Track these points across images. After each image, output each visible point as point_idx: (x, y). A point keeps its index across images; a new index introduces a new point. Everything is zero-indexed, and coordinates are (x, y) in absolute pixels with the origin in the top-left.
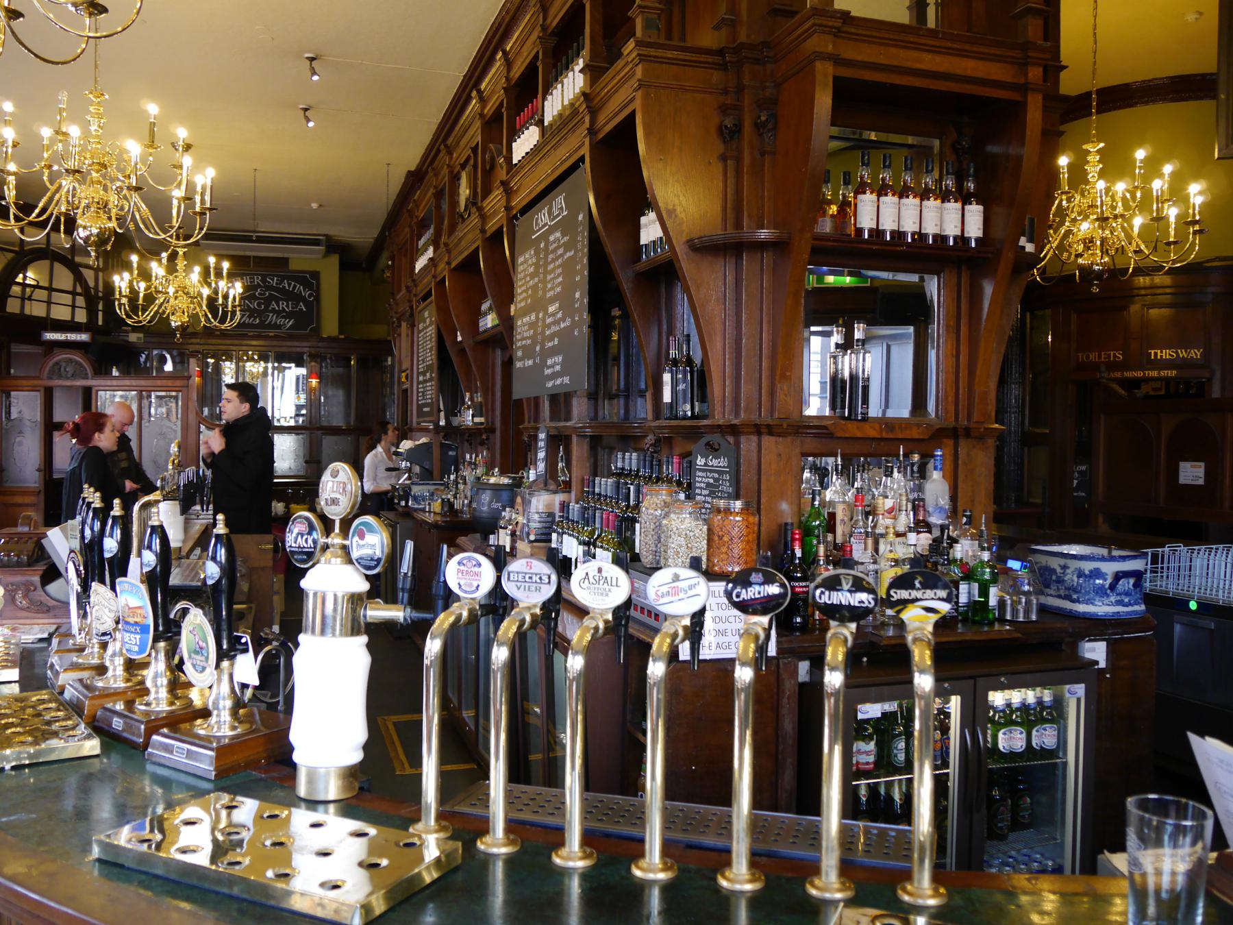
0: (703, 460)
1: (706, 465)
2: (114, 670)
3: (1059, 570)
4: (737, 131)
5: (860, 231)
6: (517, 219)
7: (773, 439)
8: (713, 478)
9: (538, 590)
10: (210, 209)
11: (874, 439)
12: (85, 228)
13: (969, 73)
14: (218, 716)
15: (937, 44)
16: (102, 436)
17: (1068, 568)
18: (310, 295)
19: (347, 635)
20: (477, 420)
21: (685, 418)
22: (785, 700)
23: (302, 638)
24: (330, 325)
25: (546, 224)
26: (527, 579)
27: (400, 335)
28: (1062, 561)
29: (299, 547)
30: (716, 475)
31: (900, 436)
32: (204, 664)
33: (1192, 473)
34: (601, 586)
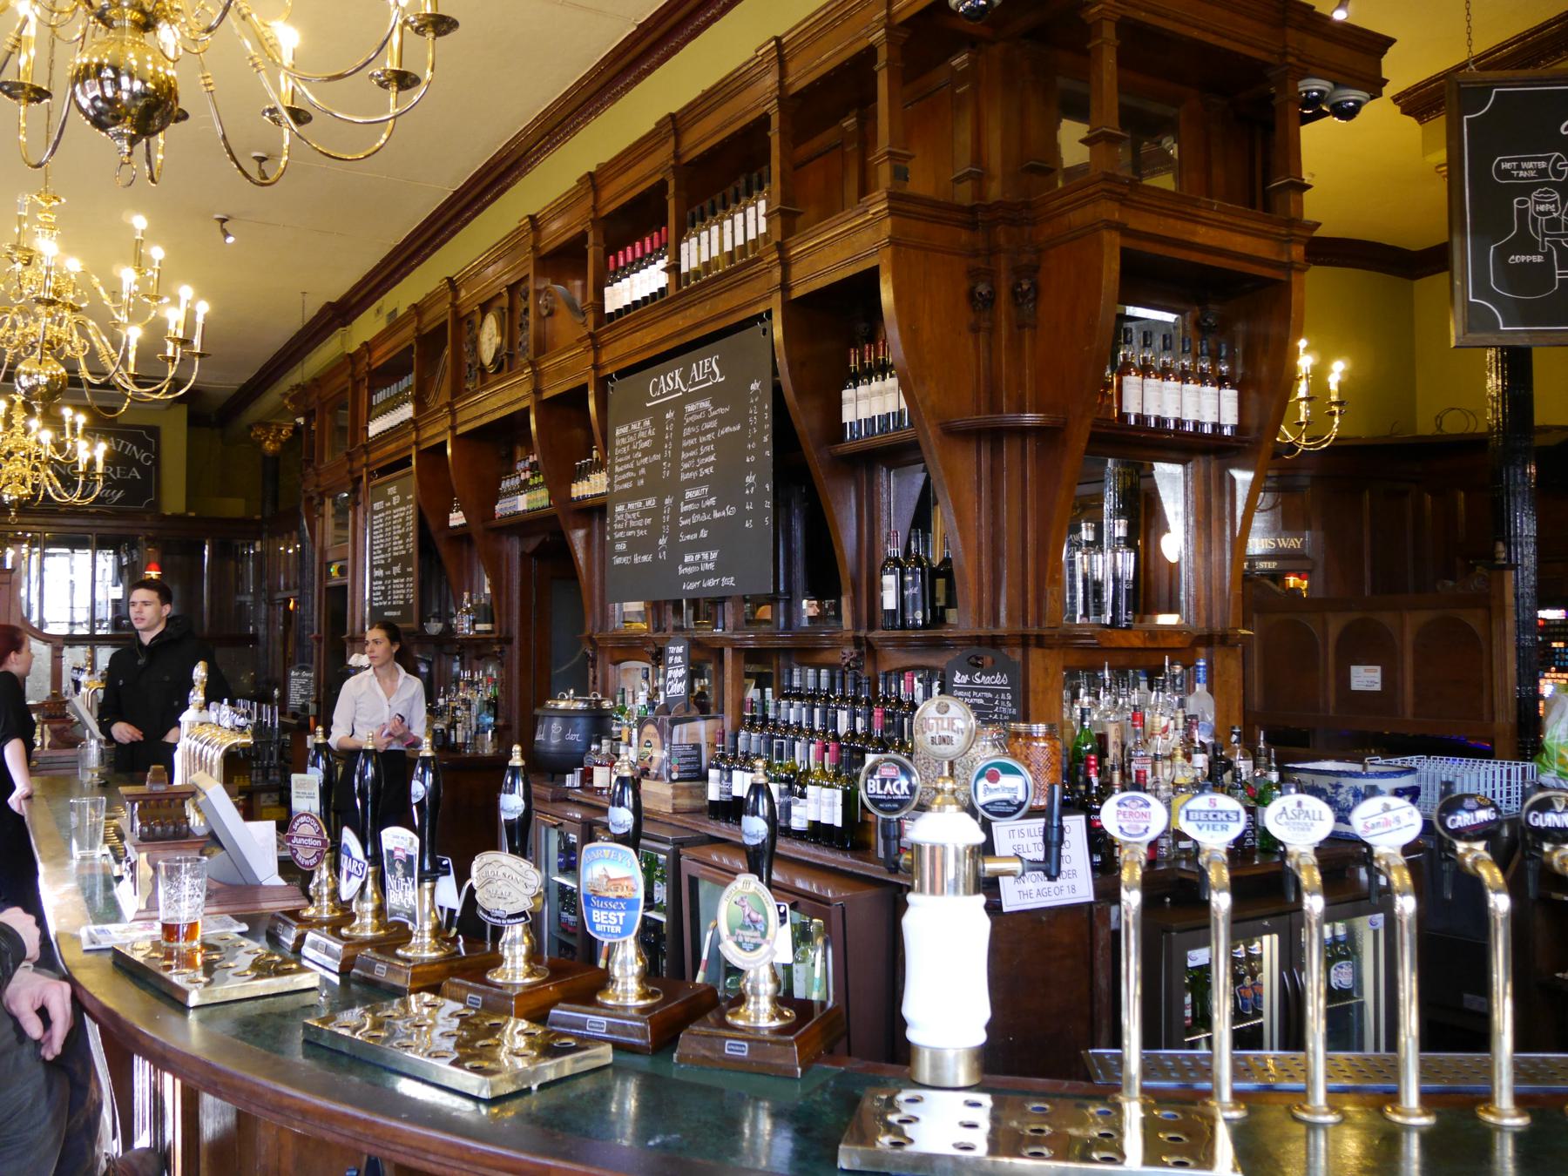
0: (965, 678)
1: (969, 682)
2: (514, 961)
3: (1329, 790)
4: (990, 301)
5: (1124, 417)
6: (613, 381)
7: (1040, 651)
8: (984, 698)
9: (1225, 828)
10: (201, 355)
11: (1139, 649)
12: (30, 375)
13: (1238, 249)
14: (756, 1003)
15: (1211, 216)
16: (18, 656)
17: (1341, 786)
18: (147, 459)
19: (969, 894)
20: (479, 627)
21: (915, 627)
22: (1099, 952)
23: (911, 898)
24: (174, 500)
25: (679, 390)
26: (1211, 817)
27: (322, 516)
28: (1334, 780)
29: (888, 794)
30: (989, 695)
31: (1162, 646)
32: (759, 940)
33: (1365, 678)
34: (1301, 821)
